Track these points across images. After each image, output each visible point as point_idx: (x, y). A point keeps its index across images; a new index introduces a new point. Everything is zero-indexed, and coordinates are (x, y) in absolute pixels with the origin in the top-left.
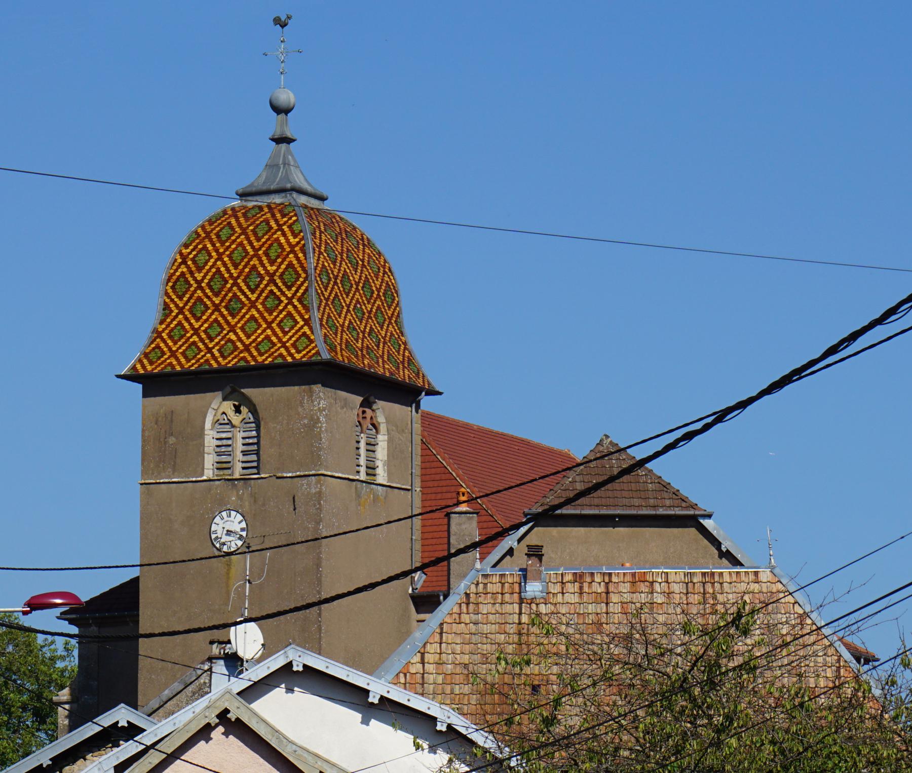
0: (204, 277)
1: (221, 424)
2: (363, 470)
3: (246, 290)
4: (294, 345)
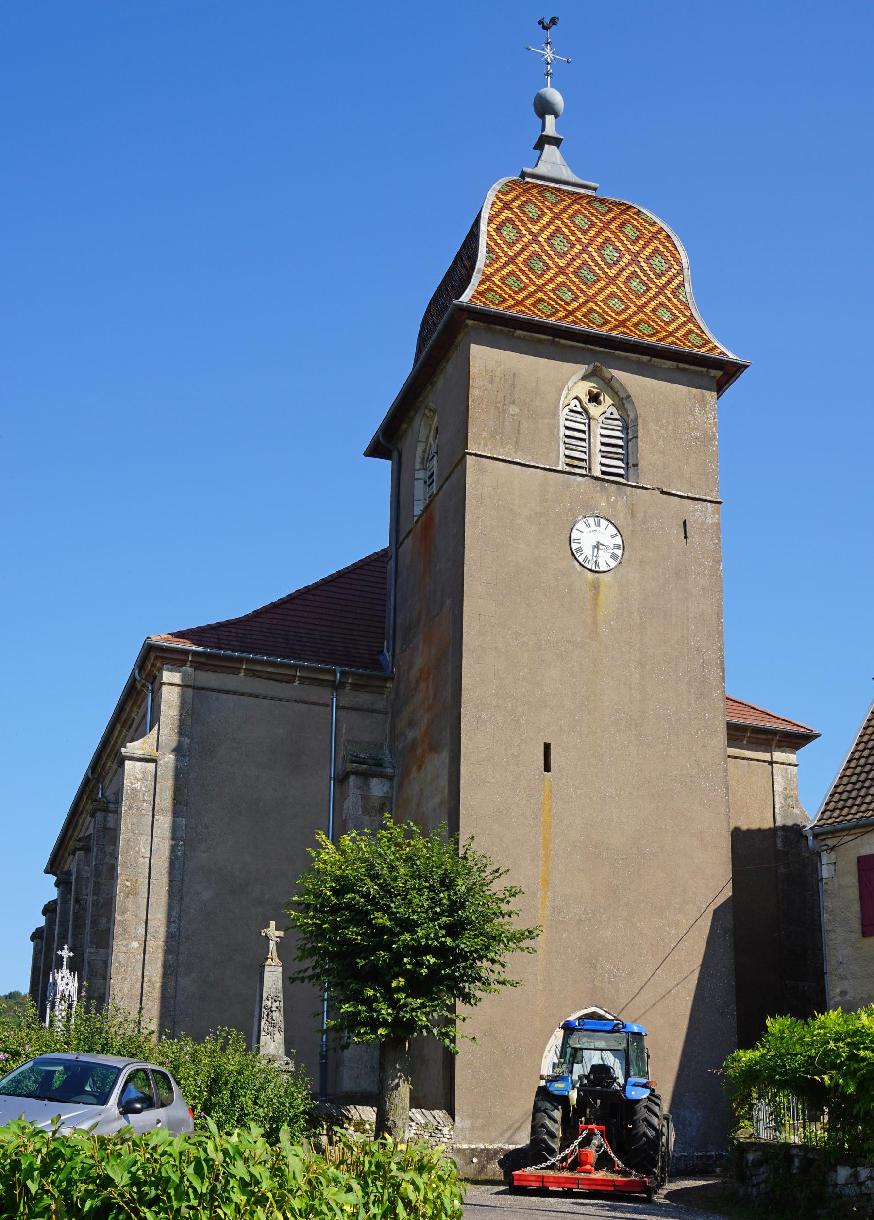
1: (571, 411)
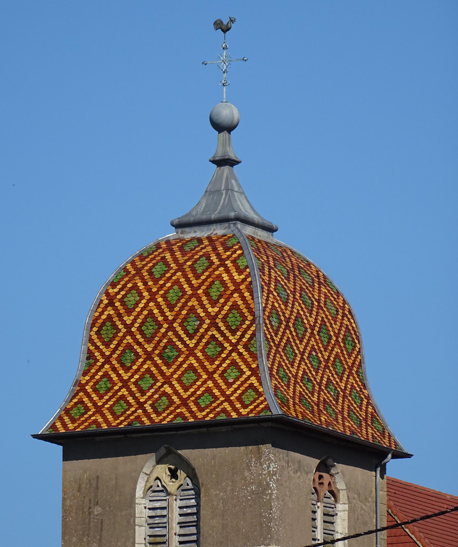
0: (134, 321)
1: (154, 491)
4: (239, 399)
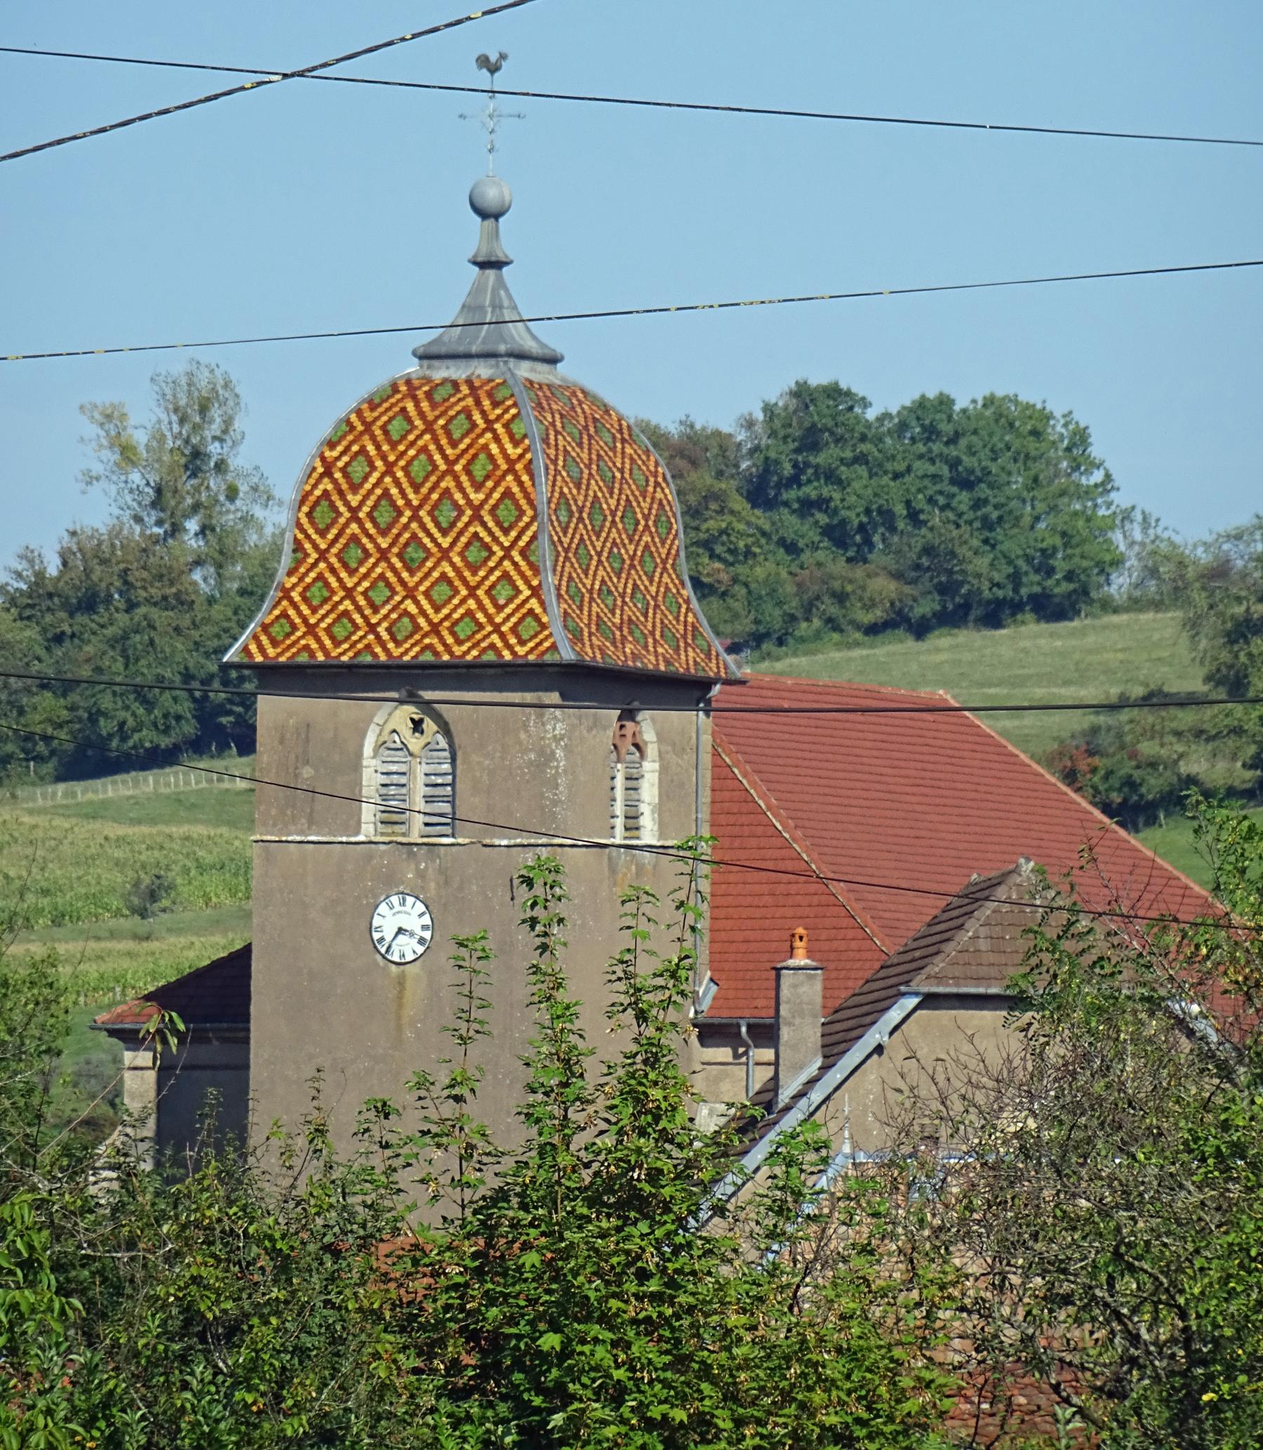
0: (362, 503)
2: (619, 823)
3: (434, 531)
4: (514, 630)
